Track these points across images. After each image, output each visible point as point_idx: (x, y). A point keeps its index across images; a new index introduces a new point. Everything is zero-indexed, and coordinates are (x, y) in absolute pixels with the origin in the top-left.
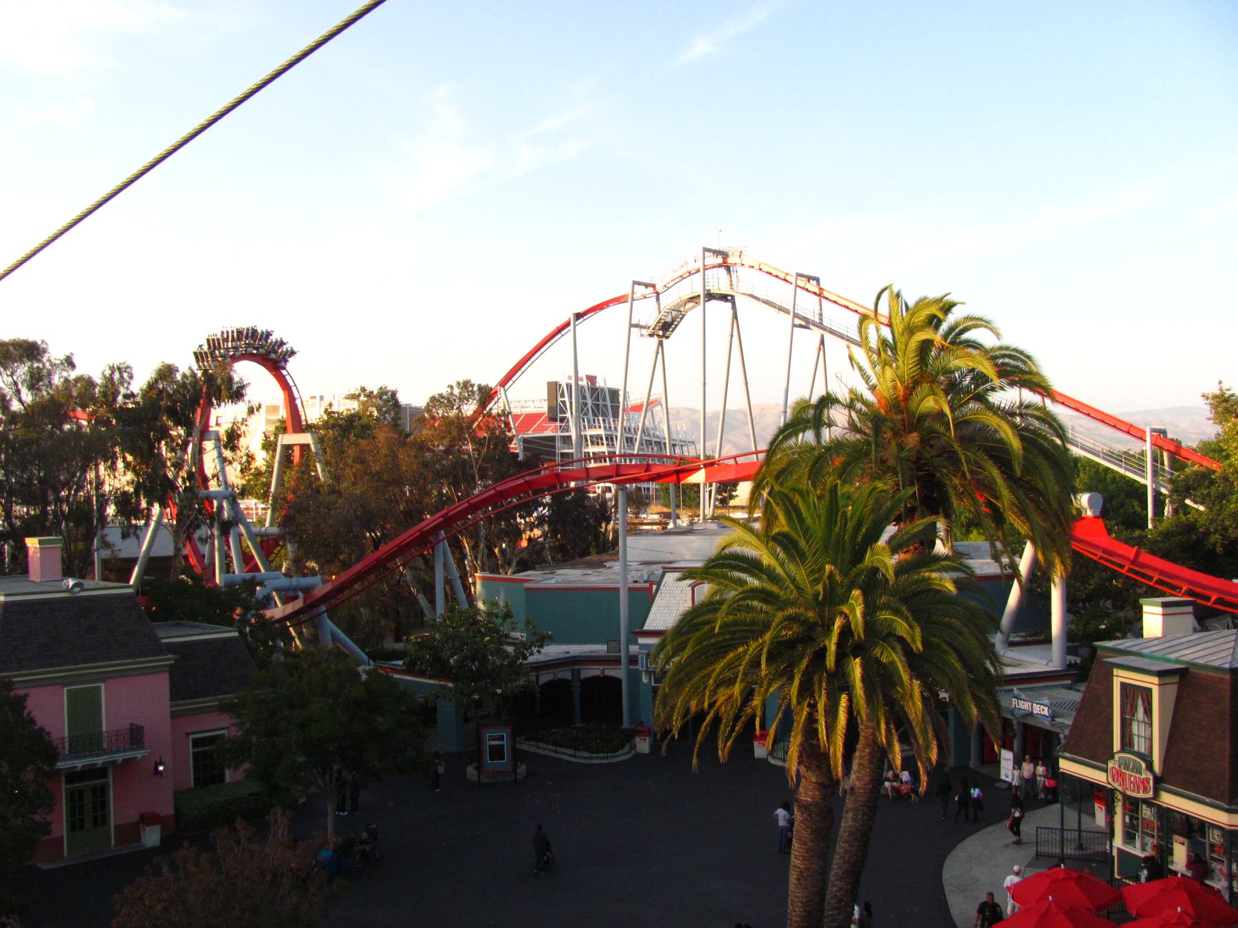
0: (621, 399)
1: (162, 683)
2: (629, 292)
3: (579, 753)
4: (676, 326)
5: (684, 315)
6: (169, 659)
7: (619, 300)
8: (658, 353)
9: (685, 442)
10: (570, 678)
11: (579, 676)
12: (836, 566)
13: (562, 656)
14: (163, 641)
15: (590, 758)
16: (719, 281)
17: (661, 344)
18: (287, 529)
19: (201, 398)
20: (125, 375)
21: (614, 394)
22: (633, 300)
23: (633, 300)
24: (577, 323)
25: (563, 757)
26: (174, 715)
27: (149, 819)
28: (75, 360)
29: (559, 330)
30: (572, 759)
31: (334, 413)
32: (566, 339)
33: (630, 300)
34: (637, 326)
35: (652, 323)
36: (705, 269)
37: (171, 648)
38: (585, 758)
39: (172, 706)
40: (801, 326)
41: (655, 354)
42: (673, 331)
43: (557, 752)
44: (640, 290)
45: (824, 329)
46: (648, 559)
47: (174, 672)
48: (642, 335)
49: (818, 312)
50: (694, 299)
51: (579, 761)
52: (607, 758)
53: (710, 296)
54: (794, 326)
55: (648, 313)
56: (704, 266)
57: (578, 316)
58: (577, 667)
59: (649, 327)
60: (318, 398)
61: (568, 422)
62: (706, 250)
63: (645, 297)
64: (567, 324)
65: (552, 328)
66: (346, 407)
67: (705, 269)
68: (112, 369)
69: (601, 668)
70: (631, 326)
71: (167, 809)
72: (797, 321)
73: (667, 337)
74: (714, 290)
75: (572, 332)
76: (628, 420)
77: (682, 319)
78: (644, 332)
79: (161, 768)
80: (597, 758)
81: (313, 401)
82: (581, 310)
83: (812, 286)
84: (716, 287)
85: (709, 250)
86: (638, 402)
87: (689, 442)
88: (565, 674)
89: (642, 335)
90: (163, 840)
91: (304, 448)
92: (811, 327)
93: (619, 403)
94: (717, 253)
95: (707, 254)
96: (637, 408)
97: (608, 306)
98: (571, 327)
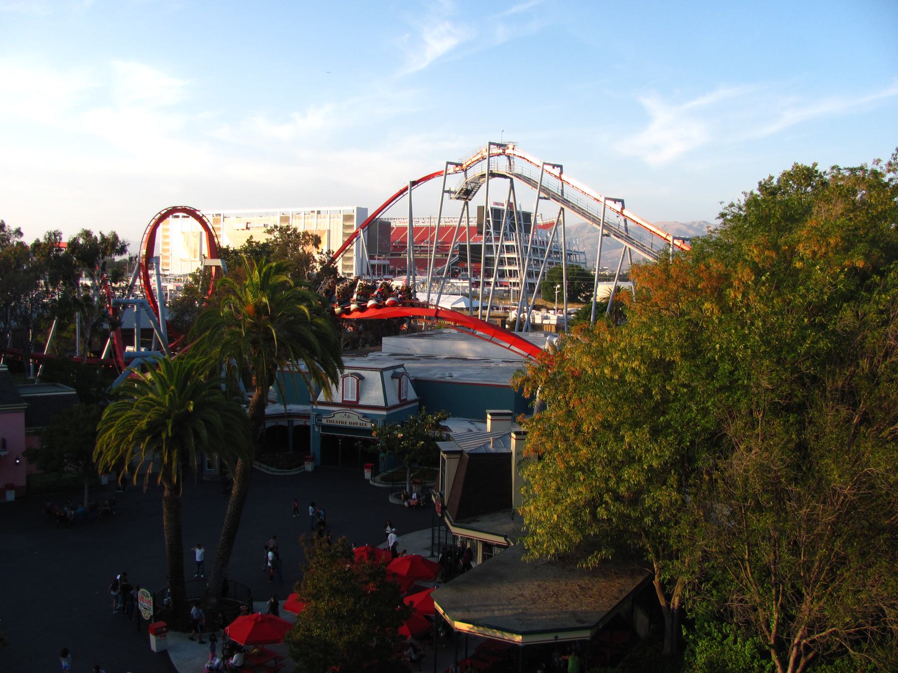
0: (532, 218)
1: (21, 418)
2: (444, 170)
3: (270, 468)
4: (476, 192)
5: (480, 186)
6: (25, 405)
7: (439, 174)
8: (464, 209)
9: (577, 252)
10: (287, 425)
11: (293, 424)
12: (177, 388)
13: (302, 412)
14: (22, 395)
15: (275, 472)
16: (500, 163)
17: (466, 204)
18: (398, 283)
19: (100, 253)
20: (58, 238)
21: (527, 216)
22: (446, 174)
23: (446, 174)
24: (412, 188)
25: (263, 470)
26: (27, 435)
27: (10, 487)
28: (22, 231)
29: (401, 192)
30: (265, 471)
31: (252, 242)
32: (405, 199)
33: (444, 173)
34: (449, 192)
35: (458, 190)
36: (490, 157)
37: (27, 399)
38: (272, 471)
39: (26, 430)
40: (545, 198)
41: (461, 211)
42: (473, 196)
43: (260, 467)
44: (451, 168)
45: (566, 202)
46: (395, 352)
47: (27, 413)
48: (451, 198)
49: (560, 188)
50: (483, 176)
51: (269, 472)
52: (284, 472)
53: (493, 175)
54: (539, 198)
55: (456, 182)
56: (489, 154)
57: (414, 183)
58: (291, 419)
59: (456, 193)
60: (316, 212)
61: (491, 235)
62: (490, 144)
63: (457, 173)
64: (406, 189)
66: (261, 238)
67: (490, 157)
68: (50, 234)
69: (304, 420)
70: (444, 191)
71: (21, 482)
72: (542, 195)
73: (470, 200)
74: (495, 171)
75: (409, 194)
76: (537, 234)
77: (479, 188)
78: (453, 196)
79: (18, 461)
80: (278, 472)
81: (313, 214)
82: (416, 179)
83: (556, 171)
84: (496, 169)
85: (494, 144)
86: (547, 220)
87: (581, 252)
88: (284, 423)
89: (451, 198)
90: (16, 498)
91: (217, 267)
92: (551, 199)
93: (531, 222)
94: (499, 146)
95: (492, 146)
96: (547, 226)
97: (433, 177)
98: (408, 191)
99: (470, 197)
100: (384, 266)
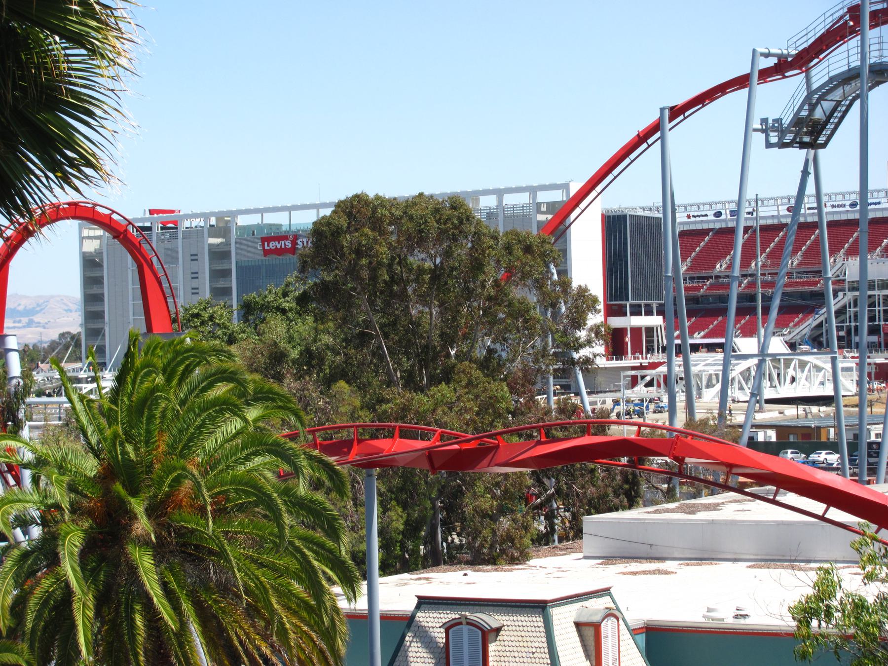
29: (642, 138)
32: (650, 156)
57: (676, 112)
65: (630, 135)
73: (824, 145)
99: (821, 140)
100: (650, 330)
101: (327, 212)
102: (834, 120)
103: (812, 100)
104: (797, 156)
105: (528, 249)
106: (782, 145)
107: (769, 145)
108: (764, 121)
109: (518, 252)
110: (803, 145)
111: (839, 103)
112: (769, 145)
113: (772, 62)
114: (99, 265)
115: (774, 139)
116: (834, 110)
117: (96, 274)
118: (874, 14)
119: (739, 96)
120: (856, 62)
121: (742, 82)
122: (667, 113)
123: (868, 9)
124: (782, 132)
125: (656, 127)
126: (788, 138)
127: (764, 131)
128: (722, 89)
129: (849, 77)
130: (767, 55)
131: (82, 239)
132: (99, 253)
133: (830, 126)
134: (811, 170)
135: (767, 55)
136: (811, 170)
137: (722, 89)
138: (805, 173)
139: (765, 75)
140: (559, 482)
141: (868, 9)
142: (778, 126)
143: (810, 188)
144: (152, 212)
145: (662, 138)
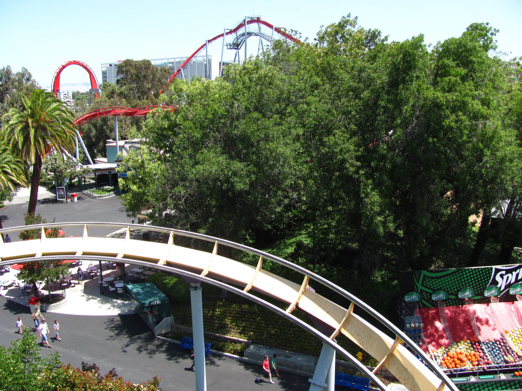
29: (202, 47)
55: (231, 39)
57: (209, 41)
65: (200, 46)
73: (240, 49)
82: (210, 39)
99: (239, 48)
101: (121, 62)
102: (241, 44)
103: (238, 39)
104: (234, 51)
105: (165, 71)
106: (231, 49)
107: (228, 49)
108: (227, 43)
109: (163, 71)
110: (235, 49)
111: (242, 40)
112: (228, 49)
113: (229, 31)
114: (106, 74)
115: (229, 47)
116: (241, 41)
117: (105, 75)
118: (248, 22)
119: (222, 38)
120: (244, 32)
121: (222, 35)
122: (207, 42)
123: (247, 20)
124: (230, 46)
125: (205, 45)
126: (232, 47)
127: (227, 46)
128: (219, 36)
129: (243, 35)
130: (228, 29)
131: (102, 67)
132: (106, 71)
133: (241, 45)
134: (237, 54)
135: (228, 29)
136: (237, 54)
137: (219, 36)
138: (236, 55)
139: (227, 34)
140: (302, 103)
141: (247, 20)
142: (230, 45)
143: (237, 59)
144: (119, 61)
145: (206, 47)
